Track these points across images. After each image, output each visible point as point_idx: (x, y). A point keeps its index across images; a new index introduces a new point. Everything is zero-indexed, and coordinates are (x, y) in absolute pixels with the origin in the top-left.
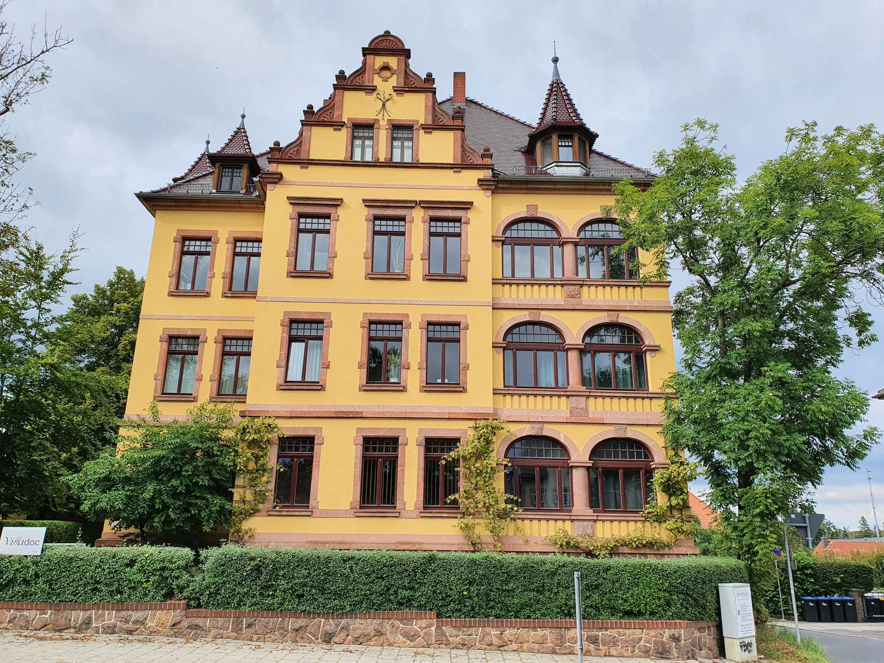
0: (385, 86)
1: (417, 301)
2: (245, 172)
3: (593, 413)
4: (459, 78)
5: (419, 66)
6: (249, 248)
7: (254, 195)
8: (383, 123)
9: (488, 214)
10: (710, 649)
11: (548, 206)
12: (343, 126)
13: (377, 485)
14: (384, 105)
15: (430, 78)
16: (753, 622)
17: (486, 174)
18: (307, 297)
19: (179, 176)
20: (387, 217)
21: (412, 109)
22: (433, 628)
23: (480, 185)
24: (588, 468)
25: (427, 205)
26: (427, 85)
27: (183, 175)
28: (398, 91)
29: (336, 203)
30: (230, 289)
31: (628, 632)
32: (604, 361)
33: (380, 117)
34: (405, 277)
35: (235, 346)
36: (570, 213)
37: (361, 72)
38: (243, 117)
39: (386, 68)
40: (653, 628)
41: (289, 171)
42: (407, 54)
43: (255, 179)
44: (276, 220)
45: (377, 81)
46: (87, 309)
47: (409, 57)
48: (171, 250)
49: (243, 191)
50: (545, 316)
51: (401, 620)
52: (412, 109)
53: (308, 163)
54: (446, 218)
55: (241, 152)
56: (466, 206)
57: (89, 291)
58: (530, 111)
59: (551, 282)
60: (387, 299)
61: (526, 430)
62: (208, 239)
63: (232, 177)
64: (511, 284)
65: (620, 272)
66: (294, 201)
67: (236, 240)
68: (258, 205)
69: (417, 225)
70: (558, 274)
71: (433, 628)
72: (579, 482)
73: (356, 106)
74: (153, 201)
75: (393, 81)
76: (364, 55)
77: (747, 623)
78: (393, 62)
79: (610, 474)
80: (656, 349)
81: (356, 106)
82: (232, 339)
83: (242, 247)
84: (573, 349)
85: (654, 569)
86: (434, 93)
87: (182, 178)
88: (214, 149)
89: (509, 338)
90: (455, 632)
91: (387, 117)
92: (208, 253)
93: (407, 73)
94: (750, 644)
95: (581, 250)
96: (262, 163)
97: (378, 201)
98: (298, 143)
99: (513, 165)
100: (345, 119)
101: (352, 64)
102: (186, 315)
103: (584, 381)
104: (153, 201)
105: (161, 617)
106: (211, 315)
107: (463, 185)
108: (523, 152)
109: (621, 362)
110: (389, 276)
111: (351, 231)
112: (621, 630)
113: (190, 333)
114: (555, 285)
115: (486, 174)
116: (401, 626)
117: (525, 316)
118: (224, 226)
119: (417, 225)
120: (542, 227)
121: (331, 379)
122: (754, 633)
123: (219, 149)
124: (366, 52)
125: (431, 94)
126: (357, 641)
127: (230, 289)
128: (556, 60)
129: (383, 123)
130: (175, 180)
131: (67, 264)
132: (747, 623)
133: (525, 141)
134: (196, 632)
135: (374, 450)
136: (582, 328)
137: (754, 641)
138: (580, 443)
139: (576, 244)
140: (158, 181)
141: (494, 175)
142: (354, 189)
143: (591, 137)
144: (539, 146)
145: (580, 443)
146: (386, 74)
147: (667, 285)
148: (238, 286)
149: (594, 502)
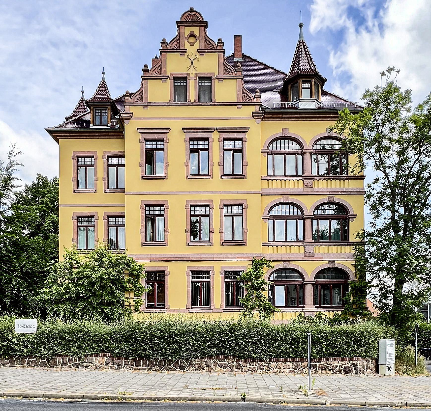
0: (191, 49)
1: (216, 190)
2: (109, 112)
3: (318, 254)
4: (238, 38)
5: (213, 34)
6: (118, 161)
7: (116, 127)
8: (192, 76)
9: (259, 135)
10: (371, 370)
11: (294, 128)
12: (167, 79)
13: (200, 296)
14: (192, 63)
15: (220, 43)
16: (394, 357)
17: (257, 108)
18: (153, 191)
19: (68, 116)
20: (198, 142)
21: (210, 65)
22: (235, 363)
23: (253, 116)
24: (313, 284)
25: (221, 130)
26: (219, 48)
27: (71, 114)
28: (201, 52)
29: (166, 131)
30: (108, 188)
31: (331, 363)
32: (324, 225)
33: (190, 72)
34: (208, 177)
35: (116, 221)
36: (309, 132)
37: (177, 39)
38: (103, 73)
39: (192, 36)
40: (344, 360)
41: (137, 111)
42: (205, 24)
43: (117, 117)
44: (133, 146)
45: (187, 45)
46: (22, 201)
47: (206, 27)
48: (71, 164)
49: (109, 125)
50: (292, 199)
51: (219, 360)
52: (210, 65)
53: (147, 105)
54: (234, 140)
55: (106, 98)
56: (245, 130)
57: (22, 189)
58: (286, 67)
59: (296, 178)
60: (200, 191)
61: (281, 265)
62: (92, 157)
63: (101, 115)
64: (272, 180)
65: (337, 170)
66: (142, 131)
67: (108, 157)
68: (119, 134)
69: (216, 143)
70: (300, 173)
71: (235, 363)
72: (309, 291)
73: (175, 65)
74: (56, 133)
75: (197, 45)
76: (178, 26)
77: (392, 357)
78: (196, 30)
79: (325, 287)
80: (354, 216)
81: (175, 65)
82: (112, 217)
83: (112, 161)
84: (308, 218)
85: (345, 333)
86: (224, 53)
87: (71, 117)
88: (89, 96)
89: (271, 213)
90: (246, 364)
91: (194, 72)
92: (93, 166)
93: (207, 40)
94: (391, 367)
95: (314, 156)
96: (118, 105)
97: (191, 129)
98: (142, 93)
99: (275, 104)
100: (168, 74)
101: (171, 34)
102: (86, 204)
103: (313, 238)
104: (56, 133)
105: (101, 360)
106: (98, 204)
107: (241, 116)
108: (279, 93)
109: (335, 225)
110: (199, 177)
111: (176, 149)
112: (328, 362)
113: (88, 215)
114: (298, 180)
115: (257, 108)
116: (219, 362)
117: (281, 199)
118: (101, 147)
119: (216, 143)
120: (291, 142)
121: (170, 238)
122: (394, 362)
123: (92, 97)
124: (180, 24)
125: (203, 28)
126: (196, 369)
127: (108, 188)
128: (301, 26)
129: (192, 76)
130: (67, 119)
131: (10, 175)
132: (392, 357)
133: (280, 83)
134: (120, 367)
135: (152, 278)
136: (313, 206)
137: (393, 366)
138: (309, 270)
139: (311, 153)
140: (58, 121)
141: (263, 109)
142: (177, 121)
143: (323, 81)
144: (290, 87)
145: (309, 270)
146: (192, 40)
147: (362, 178)
148: (112, 186)
149: (316, 302)
